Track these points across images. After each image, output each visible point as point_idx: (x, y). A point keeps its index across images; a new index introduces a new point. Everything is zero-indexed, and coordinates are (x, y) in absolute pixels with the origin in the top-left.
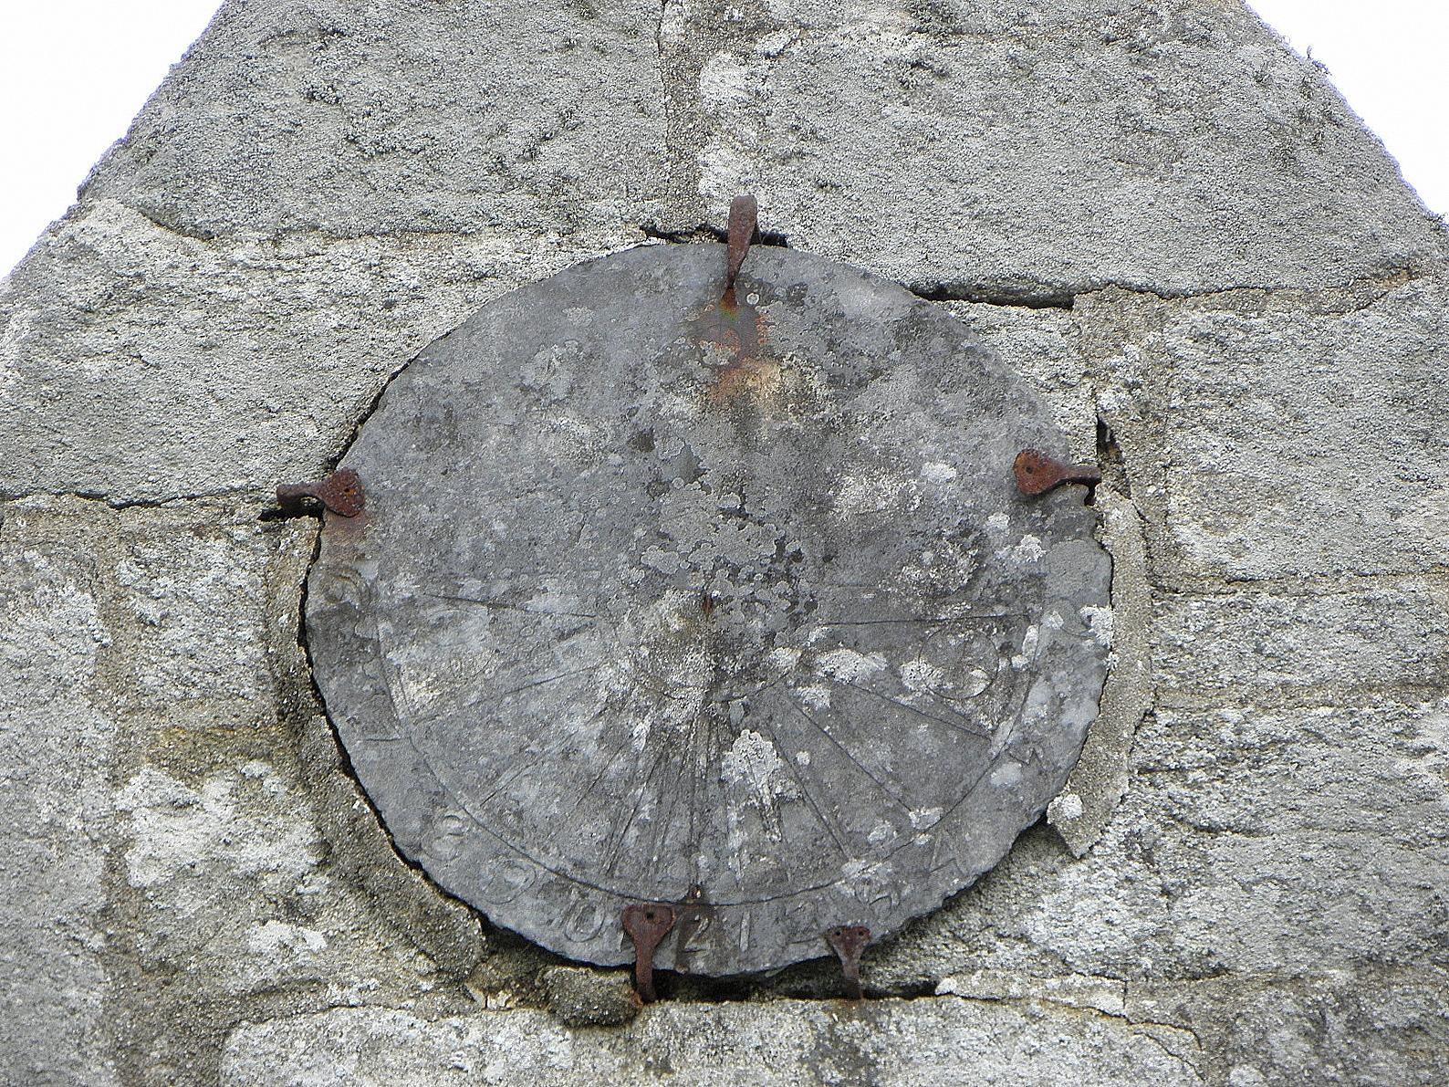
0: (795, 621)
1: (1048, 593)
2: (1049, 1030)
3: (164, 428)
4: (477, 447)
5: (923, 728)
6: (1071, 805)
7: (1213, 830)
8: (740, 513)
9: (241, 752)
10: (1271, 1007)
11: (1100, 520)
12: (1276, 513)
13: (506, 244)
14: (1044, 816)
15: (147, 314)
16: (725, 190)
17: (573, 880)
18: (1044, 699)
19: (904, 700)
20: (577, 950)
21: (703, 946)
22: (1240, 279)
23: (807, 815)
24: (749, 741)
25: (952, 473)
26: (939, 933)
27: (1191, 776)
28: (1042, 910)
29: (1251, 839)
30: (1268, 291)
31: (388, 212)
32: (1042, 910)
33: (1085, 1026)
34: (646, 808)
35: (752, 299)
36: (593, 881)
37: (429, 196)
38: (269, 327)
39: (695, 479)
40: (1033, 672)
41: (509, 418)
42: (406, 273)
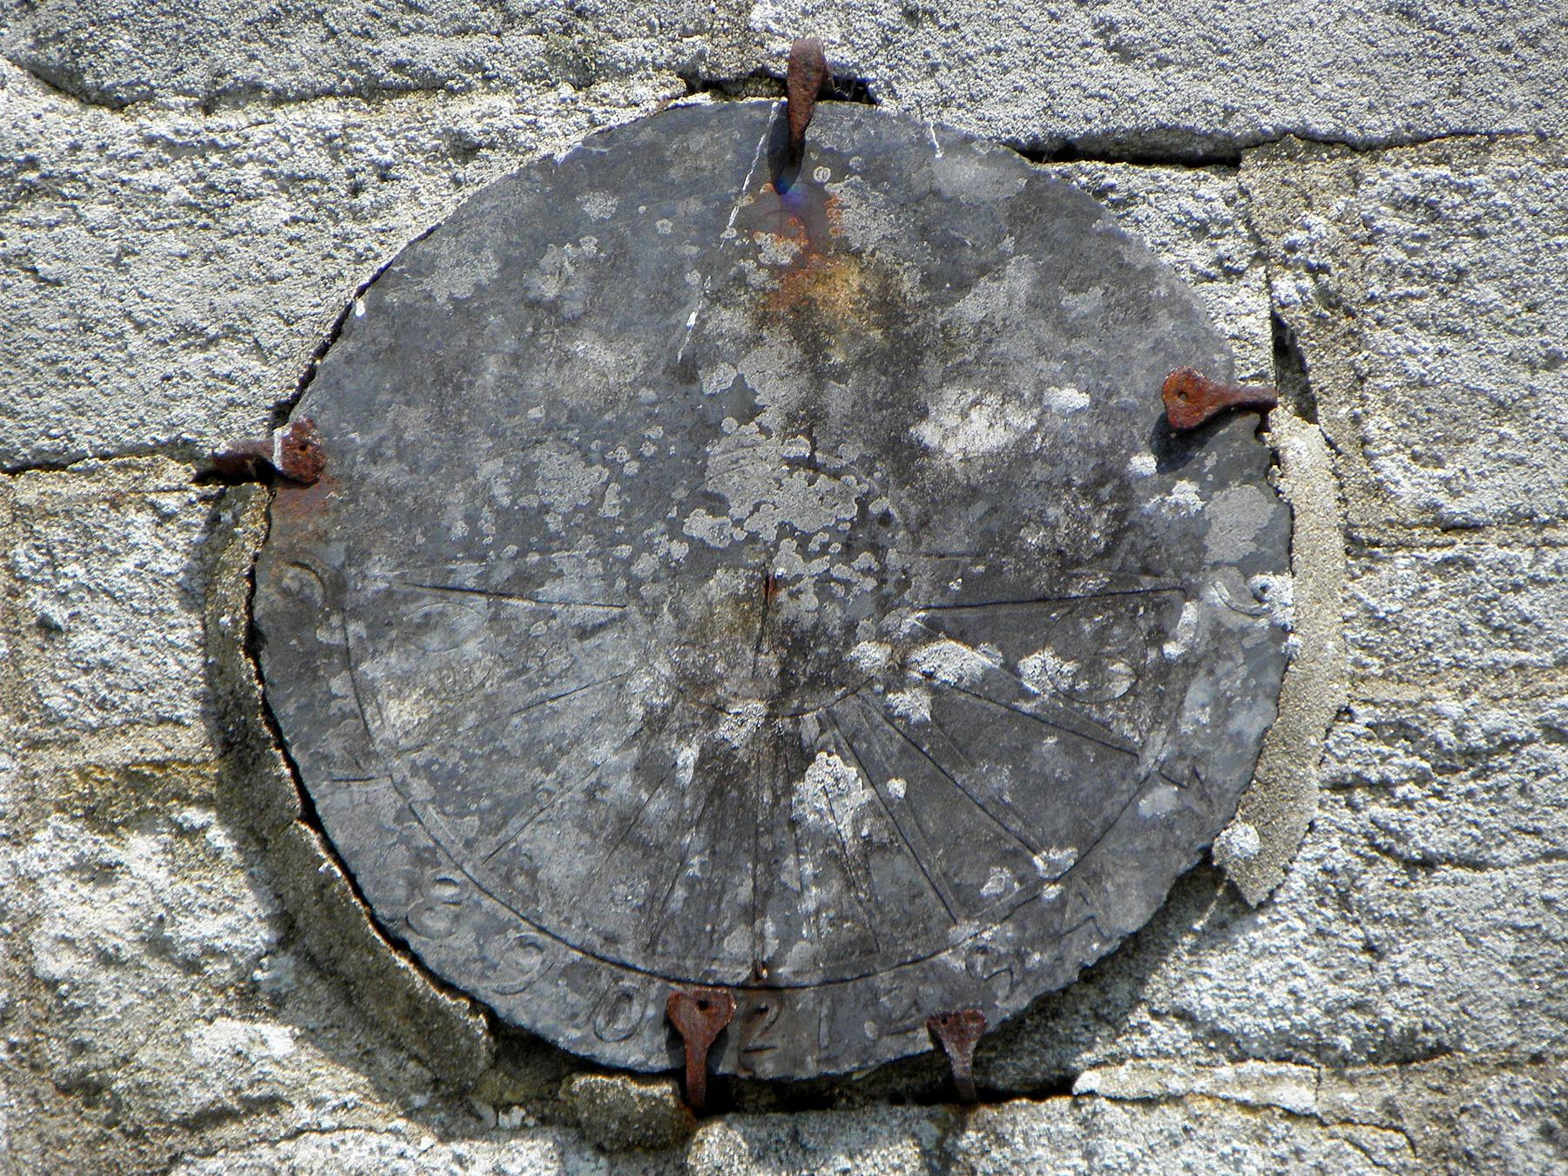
0: (884, 604)
1: (1210, 559)
2: (1218, 1137)
3: (67, 365)
4: (471, 384)
5: (1051, 741)
6: (1242, 838)
7: (1428, 863)
8: (810, 463)
9: (176, 796)
10: (1505, 1099)
11: (1275, 457)
12: (1503, 438)
13: (503, 102)
14: (1207, 853)
15: (41, 211)
16: (786, 21)
17: (603, 959)
18: (1206, 700)
19: (1027, 707)
20: (608, 1052)
21: (773, 1043)
22: (1456, 123)
23: (900, 863)
24: (828, 768)
25: (1082, 400)
26: (1077, 1012)
27: (1400, 791)
28: (1208, 977)
29: (1478, 875)
30: (1492, 138)
31: (352, 65)
32: (1208, 977)
33: (1267, 1129)
34: (695, 861)
35: (821, 174)
36: (629, 960)
37: (404, 40)
38: (200, 222)
39: (752, 419)
40: (1191, 664)
41: (509, 343)
42: (375, 145)
